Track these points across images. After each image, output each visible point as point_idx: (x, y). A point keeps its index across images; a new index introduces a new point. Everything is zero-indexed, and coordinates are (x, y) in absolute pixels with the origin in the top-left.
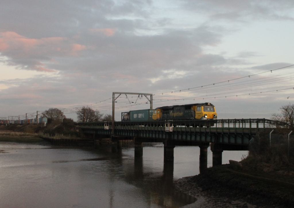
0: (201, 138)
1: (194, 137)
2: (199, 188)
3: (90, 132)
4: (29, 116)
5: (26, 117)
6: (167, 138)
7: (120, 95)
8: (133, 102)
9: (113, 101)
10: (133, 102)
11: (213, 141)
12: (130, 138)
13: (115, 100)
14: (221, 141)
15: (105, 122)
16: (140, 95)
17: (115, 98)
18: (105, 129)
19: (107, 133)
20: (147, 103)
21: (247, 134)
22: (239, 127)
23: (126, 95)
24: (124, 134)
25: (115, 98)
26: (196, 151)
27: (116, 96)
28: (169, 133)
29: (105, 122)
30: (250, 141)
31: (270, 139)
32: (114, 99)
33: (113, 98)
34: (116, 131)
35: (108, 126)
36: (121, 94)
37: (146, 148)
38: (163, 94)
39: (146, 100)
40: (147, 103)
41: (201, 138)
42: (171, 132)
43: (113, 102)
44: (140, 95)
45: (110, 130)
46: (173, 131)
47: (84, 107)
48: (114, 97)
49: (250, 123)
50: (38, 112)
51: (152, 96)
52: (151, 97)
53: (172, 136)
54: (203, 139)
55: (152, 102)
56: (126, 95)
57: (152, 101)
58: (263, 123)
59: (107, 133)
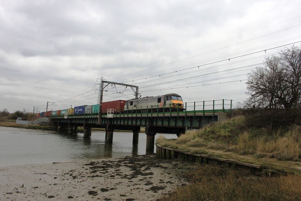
0: (128, 122)
1: (131, 121)
3: (94, 122)
6: (84, 122)
11: (147, 124)
12: (81, 125)
14: (113, 123)
17: (104, 87)
19: (91, 122)
21: (139, 117)
22: (194, 109)
24: (74, 122)
25: (104, 87)
26: (129, 136)
28: (110, 119)
36: (109, 83)
37: (116, 131)
38: (199, 68)
41: (128, 122)
47: (5, 109)
51: (138, 88)
52: (137, 89)
53: (155, 122)
54: (134, 123)
59: (91, 122)
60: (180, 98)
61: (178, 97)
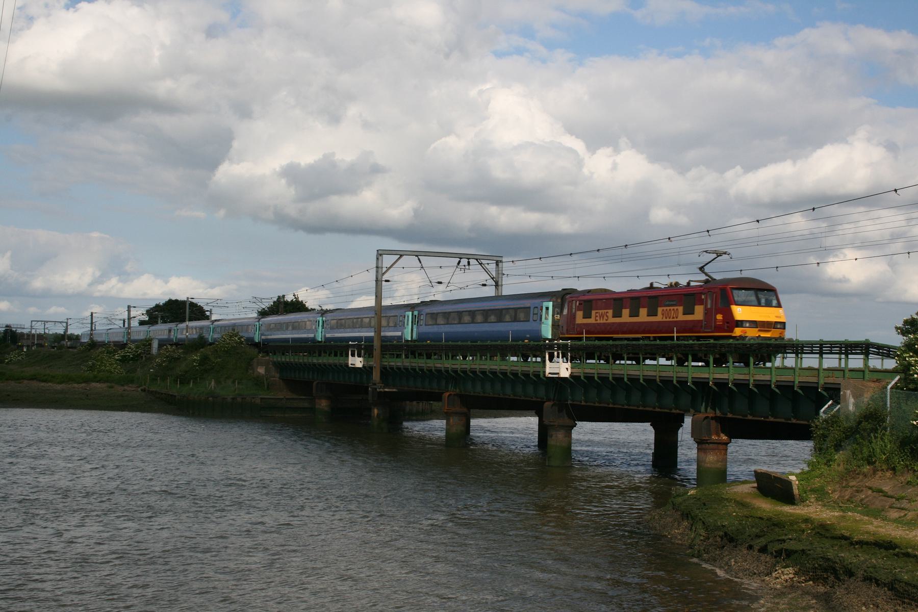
2: (495, 448)
4: (100, 322)
5: (92, 323)
7: (399, 258)
8: (440, 283)
9: (377, 278)
10: (440, 283)
13: (383, 274)
15: (350, 343)
16: (464, 262)
17: (384, 270)
18: (350, 366)
20: (484, 285)
23: (419, 259)
27: (387, 260)
28: (558, 382)
29: (350, 343)
30: (263, 319)
31: (888, 406)
32: (380, 270)
33: (377, 267)
34: (386, 373)
35: (359, 356)
36: (401, 256)
39: (483, 277)
40: (484, 285)
42: (565, 379)
43: (377, 281)
44: (464, 262)
45: (366, 371)
46: (571, 375)
48: (380, 266)
49: (867, 354)
50: (132, 309)
55: (500, 283)
56: (419, 259)
57: (500, 279)
58: (861, 354)
60: (771, 293)
61: (759, 292)
